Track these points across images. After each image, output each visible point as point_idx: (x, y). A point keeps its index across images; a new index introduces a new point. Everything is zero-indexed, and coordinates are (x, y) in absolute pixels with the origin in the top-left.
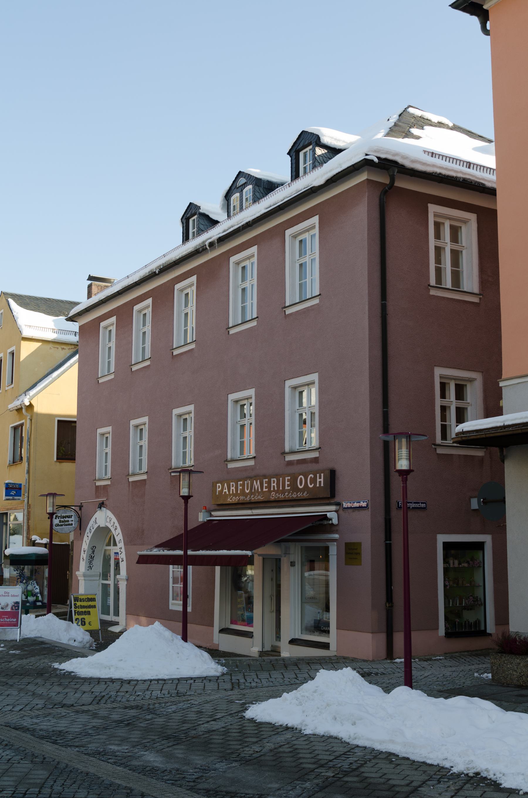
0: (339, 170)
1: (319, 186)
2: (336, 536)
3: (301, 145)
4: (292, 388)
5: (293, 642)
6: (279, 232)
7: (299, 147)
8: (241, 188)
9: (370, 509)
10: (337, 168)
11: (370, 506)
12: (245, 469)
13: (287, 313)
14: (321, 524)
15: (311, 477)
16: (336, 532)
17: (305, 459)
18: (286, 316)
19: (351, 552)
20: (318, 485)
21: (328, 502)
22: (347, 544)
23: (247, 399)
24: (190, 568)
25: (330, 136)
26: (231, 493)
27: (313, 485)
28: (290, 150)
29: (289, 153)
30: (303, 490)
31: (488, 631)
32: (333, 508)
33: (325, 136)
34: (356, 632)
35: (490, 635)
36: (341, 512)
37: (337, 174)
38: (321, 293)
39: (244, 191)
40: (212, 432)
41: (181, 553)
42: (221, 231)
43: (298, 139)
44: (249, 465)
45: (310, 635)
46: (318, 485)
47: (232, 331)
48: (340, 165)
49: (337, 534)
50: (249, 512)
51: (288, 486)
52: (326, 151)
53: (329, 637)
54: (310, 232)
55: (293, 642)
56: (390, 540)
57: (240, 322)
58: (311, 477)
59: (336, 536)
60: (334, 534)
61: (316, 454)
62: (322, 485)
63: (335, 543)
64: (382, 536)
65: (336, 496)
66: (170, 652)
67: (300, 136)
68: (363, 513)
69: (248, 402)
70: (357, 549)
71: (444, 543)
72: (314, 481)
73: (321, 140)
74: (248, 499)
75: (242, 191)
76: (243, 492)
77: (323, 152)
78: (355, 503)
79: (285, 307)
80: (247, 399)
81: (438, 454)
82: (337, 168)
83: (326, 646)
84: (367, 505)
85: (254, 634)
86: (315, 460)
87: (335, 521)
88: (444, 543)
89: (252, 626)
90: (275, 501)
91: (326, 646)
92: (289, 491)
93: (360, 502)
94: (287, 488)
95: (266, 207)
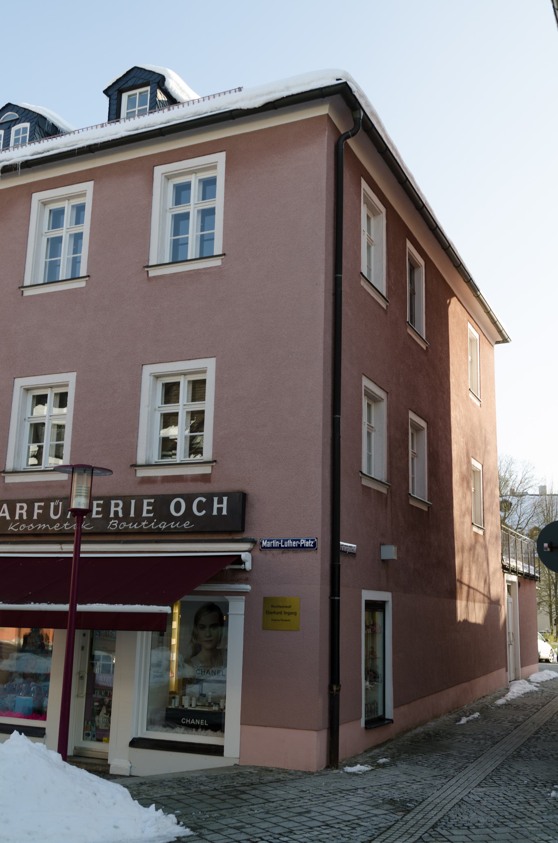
0: (285, 94)
1: (248, 109)
2: (248, 587)
3: (130, 83)
4: (154, 376)
5: (136, 743)
6: (146, 167)
7: (126, 86)
8: (10, 123)
9: (319, 550)
10: (283, 91)
11: (319, 546)
12: (48, 485)
13: (150, 275)
14: (226, 569)
15: (200, 502)
16: (246, 581)
17: (180, 476)
18: (149, 279)
19: (271, 613)
20: (215, 513)
21: (230, 538)
22: (266, 600)
23: (51, 387)
24: (78, 633)
25: (176, 84)
26: (17, 518)
27: (204, 512)
28: (109, 88)
29: (106, 92)
30: (182, 519)
31: (387, 716)
32: (247, 546)
33: (172, 78)
34: (288, 730)
35: (391, 721)
36: (257, 552)
37: (302, 93)
38: (226, 253)
39: (14, 129)
40: (107, 412)
41: (65, 607)
42: (28, 154)
43: (124, 76)
44: (56, 479)
45: (167, 731)
46: (215, 513)
47: (28, 293)
48: (288, 88)
49: (246, 584)
50: (56, 547)
51: (148, 512)
52: (166, 99)
53: (223, 736)
54: (198, 175)
55: (136, 743)
56: (339, 596)
57: (42, 282)
58: (200, 502)
59: (248, 587)
60: (239, 584)
61: (207, 470)
62: (224, 512)
63: (244, 597)
64: (327, 588)
65: (246, 529)
66: (81, 793)
67: (128, 73)
68: (302, 556)
69: (52, 391)
70: (290, 607)
71: (366, 601)
72: (208, 506)
73: (166, 83)
74: (56, 527)
75: (9, 128)
76: (44, 517)
77: (164, 99)
78: (290, 542)
79: (148, 267)
80: (51, 387)
81: (362, 485)
82: (283, 91)
83: (218, 750)
84: (314, 544)
85: (46, 731)
86: (205, 478)
87: (248, 566)
88: (366, 601)
89: (45, 719)
90: (118, 533)
91: (218, 750)
92: (150, 520)
93: (299, 541)
94: (145, 514)
95: (130, 129)
